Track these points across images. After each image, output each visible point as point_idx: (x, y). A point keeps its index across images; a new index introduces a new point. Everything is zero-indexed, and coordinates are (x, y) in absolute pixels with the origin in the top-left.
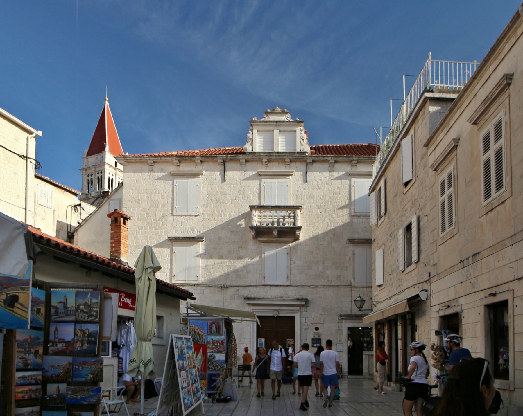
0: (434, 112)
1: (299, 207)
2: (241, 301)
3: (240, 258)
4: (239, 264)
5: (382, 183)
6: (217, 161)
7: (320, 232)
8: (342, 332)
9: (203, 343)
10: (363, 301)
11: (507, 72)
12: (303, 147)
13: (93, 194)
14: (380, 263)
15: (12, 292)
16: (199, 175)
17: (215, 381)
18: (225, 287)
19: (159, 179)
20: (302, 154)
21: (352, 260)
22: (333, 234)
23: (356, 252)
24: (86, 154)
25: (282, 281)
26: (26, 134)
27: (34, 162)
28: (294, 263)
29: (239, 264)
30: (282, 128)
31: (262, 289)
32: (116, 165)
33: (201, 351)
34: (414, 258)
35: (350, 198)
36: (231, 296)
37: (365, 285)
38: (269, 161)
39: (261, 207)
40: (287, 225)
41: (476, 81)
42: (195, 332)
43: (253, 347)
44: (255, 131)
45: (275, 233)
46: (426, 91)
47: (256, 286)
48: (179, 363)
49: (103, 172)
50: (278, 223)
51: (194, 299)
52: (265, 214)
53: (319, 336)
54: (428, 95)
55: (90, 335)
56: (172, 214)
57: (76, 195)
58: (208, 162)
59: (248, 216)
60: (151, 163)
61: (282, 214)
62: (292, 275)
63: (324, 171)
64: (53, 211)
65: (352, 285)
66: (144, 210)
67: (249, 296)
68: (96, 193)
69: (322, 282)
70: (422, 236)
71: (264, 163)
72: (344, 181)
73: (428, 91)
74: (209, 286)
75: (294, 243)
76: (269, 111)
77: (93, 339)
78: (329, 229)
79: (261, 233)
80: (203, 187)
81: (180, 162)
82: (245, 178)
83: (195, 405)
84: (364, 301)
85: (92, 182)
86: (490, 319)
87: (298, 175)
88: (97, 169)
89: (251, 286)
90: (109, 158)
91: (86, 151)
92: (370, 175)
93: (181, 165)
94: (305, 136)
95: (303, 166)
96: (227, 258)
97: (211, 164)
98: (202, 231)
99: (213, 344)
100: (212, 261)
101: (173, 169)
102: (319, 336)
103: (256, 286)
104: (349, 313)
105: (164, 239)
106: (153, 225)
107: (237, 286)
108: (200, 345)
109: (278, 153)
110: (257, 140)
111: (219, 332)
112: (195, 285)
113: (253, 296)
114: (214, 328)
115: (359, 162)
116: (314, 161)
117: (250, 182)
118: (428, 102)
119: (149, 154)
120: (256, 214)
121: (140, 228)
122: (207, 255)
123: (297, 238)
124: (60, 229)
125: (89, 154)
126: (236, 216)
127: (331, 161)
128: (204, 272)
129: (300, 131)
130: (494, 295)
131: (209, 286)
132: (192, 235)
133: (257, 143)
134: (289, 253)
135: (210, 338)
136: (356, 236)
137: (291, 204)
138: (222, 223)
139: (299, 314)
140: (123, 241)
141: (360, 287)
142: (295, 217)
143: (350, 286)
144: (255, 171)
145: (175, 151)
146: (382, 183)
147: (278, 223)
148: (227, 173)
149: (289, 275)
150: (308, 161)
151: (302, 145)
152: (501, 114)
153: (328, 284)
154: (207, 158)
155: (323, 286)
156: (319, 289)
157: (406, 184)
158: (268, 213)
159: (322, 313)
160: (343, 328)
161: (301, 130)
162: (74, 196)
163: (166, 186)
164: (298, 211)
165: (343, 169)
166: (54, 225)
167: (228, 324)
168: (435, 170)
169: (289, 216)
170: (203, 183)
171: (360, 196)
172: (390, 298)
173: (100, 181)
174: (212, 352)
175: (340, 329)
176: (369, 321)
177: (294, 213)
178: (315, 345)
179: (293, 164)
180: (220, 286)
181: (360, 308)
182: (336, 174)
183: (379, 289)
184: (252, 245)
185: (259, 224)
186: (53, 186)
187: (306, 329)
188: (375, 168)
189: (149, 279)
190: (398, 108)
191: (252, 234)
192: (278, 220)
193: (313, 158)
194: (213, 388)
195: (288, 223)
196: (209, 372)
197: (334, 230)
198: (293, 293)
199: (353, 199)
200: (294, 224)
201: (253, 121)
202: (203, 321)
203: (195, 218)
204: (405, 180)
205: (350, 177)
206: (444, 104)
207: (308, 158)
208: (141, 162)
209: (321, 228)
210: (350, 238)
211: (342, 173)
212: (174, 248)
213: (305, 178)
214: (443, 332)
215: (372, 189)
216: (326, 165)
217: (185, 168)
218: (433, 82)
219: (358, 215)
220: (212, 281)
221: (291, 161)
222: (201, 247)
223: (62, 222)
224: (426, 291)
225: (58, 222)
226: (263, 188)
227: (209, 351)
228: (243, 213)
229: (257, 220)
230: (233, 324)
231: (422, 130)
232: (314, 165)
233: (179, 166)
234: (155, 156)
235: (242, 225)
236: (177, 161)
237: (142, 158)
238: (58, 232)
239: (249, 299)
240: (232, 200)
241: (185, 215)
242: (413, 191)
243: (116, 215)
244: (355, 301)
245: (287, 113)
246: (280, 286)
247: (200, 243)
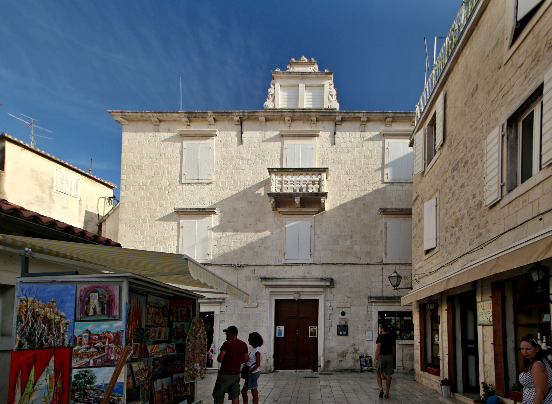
2: (258, 282)
3: (256, 231)
4: (252, 237)
5: (441, 97)
8: (371, 317)
9: (58, 343)
10: (399, 277)
12: (331, 103)
18: (240, 267)
19: (166, 140)
20: (331, 111)
21: (383, 234)
23: (388, 225)
25: (304, 258)
29: (252, 237)
30: (309, 83)
31: (281, 267)
33: (52, 364)
36: (246, 277)
37: (398, 262)
39: (282, 171)
42: (35, 316)
43: (270, 337)
44: (277, 85)
45: (297, 200)
47: (275, 265)
50: (301, 189)
53: (346, 322)
56: (181, 182)
57: (111, 187)
58: (223, 121)
60: (156, 122)
62: (316, 252)
64: (80, 201)
65: (384, 262)
66: (147, 178)
67: (267, 276)
69: (349, 260)
71: (287, 122)
74: (221, 265)
79: (281, 201)
80: (217, 151)
82: (264, 139)
87: (325, 135)
89: (270, 265)
93: (192, 124)
94: (334, 92)
95: (330, 126)
99: (91, 343)
102: (346, 322)
103: (275, 265)
104: (380, 295)
106: (158, 195)
108: (50, 347)
110: (280, 96)
111: (110, 313)
114: (95, 301)
116: (343, 120)
117: (270, 144)
120: (275, 178)
121: (142, 199)
122: (219, 228)
124: (89, 220)
126: (253, 183)
127: (362, 119)
128: (216, 249)
129: (329, 86)
135: (80, 329)
136: (389, 206)
138: (237, 192)
141: (393, 264)
142: (320, 182)
143: (381, 263)
144: (276, 131)
146: (441, 97)
148: (245, 134)
149: (312, 252)
150: (337, 119)
151: (330, 101)
153: (357, 261)
155: (351, 264)
156: (346, 267)
158: (289, 178)
159: (349, 295)
160: (373, 313)
161: (330, 85)
162: (108, 189)
164: (324, 175)
166: (80, 215)
170: (217, 146)
171: (394, 159)
174: (87, 365)
178: (341, 333)
179: (319, 124)
181: (396, 287)
182: (368, 135)
184: (271, 217)
185: (278, 191)
186: (79, 175)
187: (330, 314)
191: (270, 203)
193: (343, 114)
195: (313, 189)
198: (316, 272)
199: (386, 163)
200: (319, 189)
202: (62, 286)
203: (206, 187)
205: (383, 138)
207: (337, 114)
210: (383, 207)
212: (181, 221)
213: (333, 139)
216: (357, 125)
220: (223, 256)
221: (317, 120)
222: (213, 220)
223: (92, 213)
225: (87, 212)
226: (285, 151)
227: (75, 362)
228: (262, 180)
232: (344, 124)
233: (189, 125)
235: (261, 194)
236: (187, 119)
237: (144, 114)
238: (86, 222)
239: (265, 279)
240: (250, 165)
241: (196, 183)
244: (389, 277)
245: (314, 64)
246: (302, 264)
247: (212, 215)
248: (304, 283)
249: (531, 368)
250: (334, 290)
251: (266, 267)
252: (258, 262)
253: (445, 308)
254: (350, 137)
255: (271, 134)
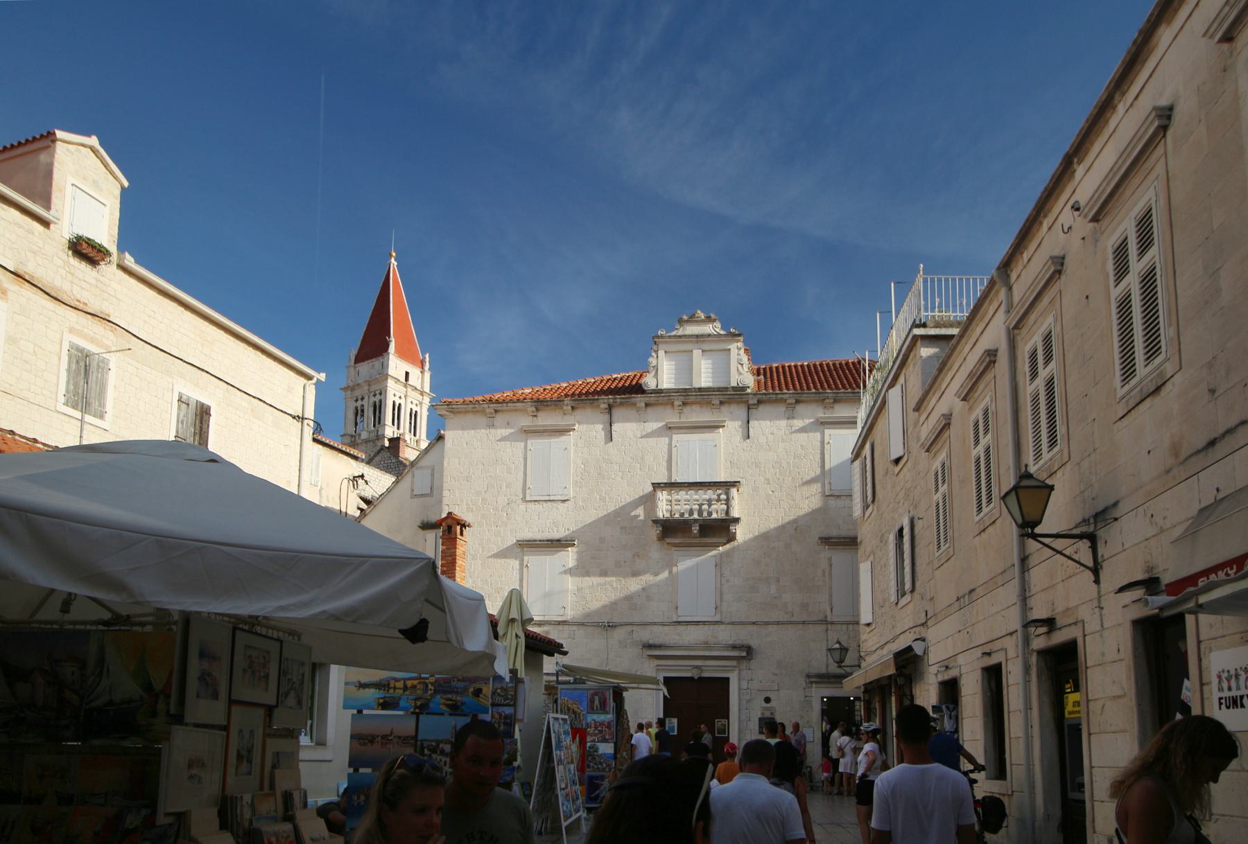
0: (929, 357)
1: (734, 484)
3: (635, 574)
4: (634, 585)
5: (868, 446)
6: (598, 406)
7: (772, 526)
10: (844, 650)
11: (988, 347)
13: (364, 435)
14: (871, 579)
15: (477, 686)
16: (569, 431)
17: (598, 787)
18: (611, 626)
19: (503, 439)
20: (740, 390)
22: (795, 528)
23: (834, 562)
24: (353, 358)
25: (708, 614)
26: (303, 381)
27: (312, 423)
28: (728, 581)
30: (706, 347)
32: (407, 379)
34: (908, 586)
35: (823, 466)
37: (848, 619)
38: (684, 404)
39: (671, 486)
40: (714, 516)
41: (964, 341)
44: (661, 353)
45: (695, 529)
46: (915, 325)
47: (663, 624)
48: (556, 753)
49: (383, 392)
50: (700, 512)
51: (565, 653)
52: (679, 497)
54: (917, 331)
55: (506, 717)
56: (524, 500)
59: (648, 501)
61: (707, 497)
63: (778, 418)
68: (370, 432)
70: (917, 549)
72: (811, 434)
73: (918, 326)
75: (728, 546)
76: (685, 317)
77: (1179, 716)
78: (787, 519)
79: (672, 530)
81: (537, 410)
83: (574, 817)
84: (847, 650)
85: (363, 411)
86: (991, 689)
87: (733, 427)
88: (373, 388)
89: (655, 624)
90: (396, 365)
91: (354, 352)
92: (852, 423)
93: (539, 414)
94: (745, 359)
95: (741, 411)
96: (613, 575)
97: (588, 412)
98: (573, 528)
100: (588, 581)
101: (526, 421)
103: (663, 624)
104: (824, 671)
105: (509, 543)
107: (631, 624)
109: (700, 389)
112: (559, 623)
113: (657, 641)
114: (597, 702)
115: (836, 401)
116: (760, 402)
117: (652, 441)
118: (919, 343)
119: (488, 397)
120: (663, 496)
122: (581, 570)
123: (732, 538)
125: (359, 359)
129: (737, 351)
130: (989, 654)
131: (583, 624)
132: (556, 535)
133: (664, 373)
134: (719, 564)
136: (834, 532)
137: (722, 477)
139: (736, 672)
140: (459, 562)
141: (842, 623)
143: (824, 621)
145: (528, 387)
146: (868, 446)
147: (700, 512)
148: (615, 427)
151: (740, 374)
152: (988, 399)
154: (584, 398)
155: (778, 623)
157: (897, 461)
158: (682, 495)
161: (739, 349)
163: (513, 451)
164: (734, 491)
165: (809, 414)
167: (618, 694)
168: (928, 451)
169: (719, 500)
170: (576, 445)
171: (840, 461)
172: (882, 647)
173: (378, 409)
175: (807, 701)
176: (852, 686)
177: (727, 494)
179: (725, 408)
180: (601, 624)
181: (840, 663)
182: (798, 423)
183: (868, 629)
184: (656, 552)
185: (667, 515)
187: (748, 701)
188: (862, 414)
189: (517, 636)
190: (888, 327)
191: (655, 532)
192: (700, 505)
194: (594, 800)
195: (717, 511)
196: (589, 772)
197: (795, 521)
198: (725, 635)
199: (827, 467)
201: (658, 337)
203: (561, 505)
204: (894, 456)
206: (943, 344)
208: (475, 412)
209: (774, 518)
211: (807, 421)
212: (526, 558)
214: (944, 707)
215: (857, 454)
216: (781, 409)
217: (547, 419)
218: (926, 310)
219: (835, 495)
220: (588, 615)
221: (722, 403)
222: (569, 557)
224: (924, 640)
226: (674, 450)
227: (589, 738)
229: (665, 507)
230: (625, 694)
231: (914, 379)
232: (761, 408)
234: (497, 402)
239: (650, 646)
242: (907, 473)
243: (449, 521)
245: (714, 321)
246: (704, 623)
248: (707, 653)
249: (265, 617)
250: (753, 664)
251: (649, 628)
252: (636, 619)
253: (877, 699)
254: (772, 429)
255: (653, 426)
